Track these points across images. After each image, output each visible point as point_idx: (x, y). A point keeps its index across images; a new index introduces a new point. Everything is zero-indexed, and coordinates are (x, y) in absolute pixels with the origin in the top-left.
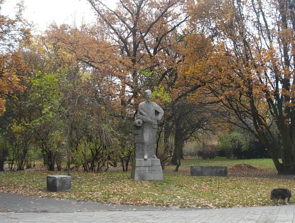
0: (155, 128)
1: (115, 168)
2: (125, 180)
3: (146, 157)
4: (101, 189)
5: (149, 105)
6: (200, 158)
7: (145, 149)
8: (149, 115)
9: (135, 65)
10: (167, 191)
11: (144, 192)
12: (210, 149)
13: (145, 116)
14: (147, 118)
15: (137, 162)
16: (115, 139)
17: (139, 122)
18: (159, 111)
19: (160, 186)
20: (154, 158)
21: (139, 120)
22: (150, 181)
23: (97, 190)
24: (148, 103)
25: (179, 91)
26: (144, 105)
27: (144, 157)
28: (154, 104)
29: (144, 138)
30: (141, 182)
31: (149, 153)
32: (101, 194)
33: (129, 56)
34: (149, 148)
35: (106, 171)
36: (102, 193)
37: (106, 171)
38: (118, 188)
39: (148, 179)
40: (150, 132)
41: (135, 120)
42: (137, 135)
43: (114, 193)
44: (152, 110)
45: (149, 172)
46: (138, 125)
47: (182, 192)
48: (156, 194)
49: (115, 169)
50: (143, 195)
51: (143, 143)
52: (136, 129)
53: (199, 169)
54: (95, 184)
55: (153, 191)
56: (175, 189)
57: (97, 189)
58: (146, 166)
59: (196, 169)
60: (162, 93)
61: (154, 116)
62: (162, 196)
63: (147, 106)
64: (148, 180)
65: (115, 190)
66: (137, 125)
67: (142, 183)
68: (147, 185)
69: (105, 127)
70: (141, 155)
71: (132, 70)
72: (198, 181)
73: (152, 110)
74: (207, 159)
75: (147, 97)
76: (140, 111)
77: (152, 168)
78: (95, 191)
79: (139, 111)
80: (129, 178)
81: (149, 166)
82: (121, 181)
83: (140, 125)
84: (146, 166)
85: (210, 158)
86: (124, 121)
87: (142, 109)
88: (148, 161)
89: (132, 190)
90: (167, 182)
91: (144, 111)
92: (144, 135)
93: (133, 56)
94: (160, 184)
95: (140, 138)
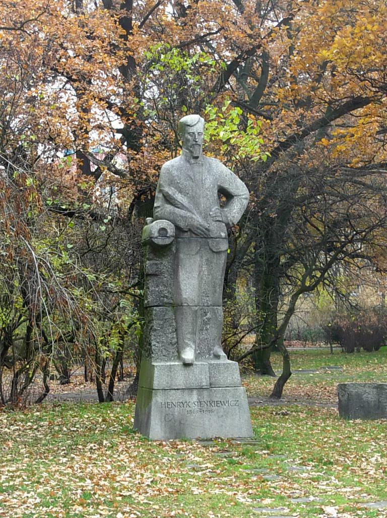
0: (219, 253)
1: (65, 387)
2: (116, 440)
3: (189, 355)
4: (35, 479)
5: (196, 169)
6: (337, 348)
7: (186, 328)
8: (197, 205)
9: (130, 37)
10: (275, 484)
11: (196, 491)
12: (374, 319)
13: (182, 207)
14: (189, 214)
15: (156, 373)
16: (77, 292)
17: (163, 231)
18: (232, 190)
19: (246, 462)
20: (217, 357)
21: (164, 223)
22: (206, 441)
23: (21, 484)
24: (192, 161)
25: (282, 125)
26: (179, 169)
27: (183, 356)
28: (214, 165)
29: (182, 287)
30: (174, 446)
31: (198, 341)
32: (38, 500)
33: (109, 8)
34: (199, 320)
35: (40, 401)
36: (39, 495)
37: (40, 401)
38: (95, 471)
39: (199, 434)
40: (201, 266)
41: (147, 224)
42: (155, 275)
43: (86, 495)
44: (207, 186)
45: (201, 411)
46: (160, 241)
47: (336, 487)
48: (240, 498)
49: (66, 390)
50: (196, 503)
51: (177, 306)
52: (151, 256)
53: (370, 396)
54: (9, 457)
55: (225, 483)
56: (305, 475)
57: (18, 481)
58: (191, 389)
59: (359, 396)
60: (235, 128)
61: (215, 208)
62: (266, 507)
63: (190, 173)
64: (197, 439)
65: (88, 481)
66: (156, 241)
67: (178, 452)
68: (197, 459)
69: (38, 248)
70: (172, 350)
71: (121, 53)
72: (375, 439)
73: (207, 186)
74: (359, 351)
75: (188, 140)
76: (166, 189)
77: (209, 396)
78: (14, 488)
79: (161, 191)
80: (126, 431)
81: (201, 389)
82: (101, 444)
83: (167, 241)
84: (191, 389)
85: (368, 350)
86: (103, 228)
87: (172, 183)
88: (195, 370)
89: (148, 482)
90: (268, 448)
91: (180, 192)
92: (183, 275)
93: (122, 8)
94: (244, 454)
95: (165, 286)
